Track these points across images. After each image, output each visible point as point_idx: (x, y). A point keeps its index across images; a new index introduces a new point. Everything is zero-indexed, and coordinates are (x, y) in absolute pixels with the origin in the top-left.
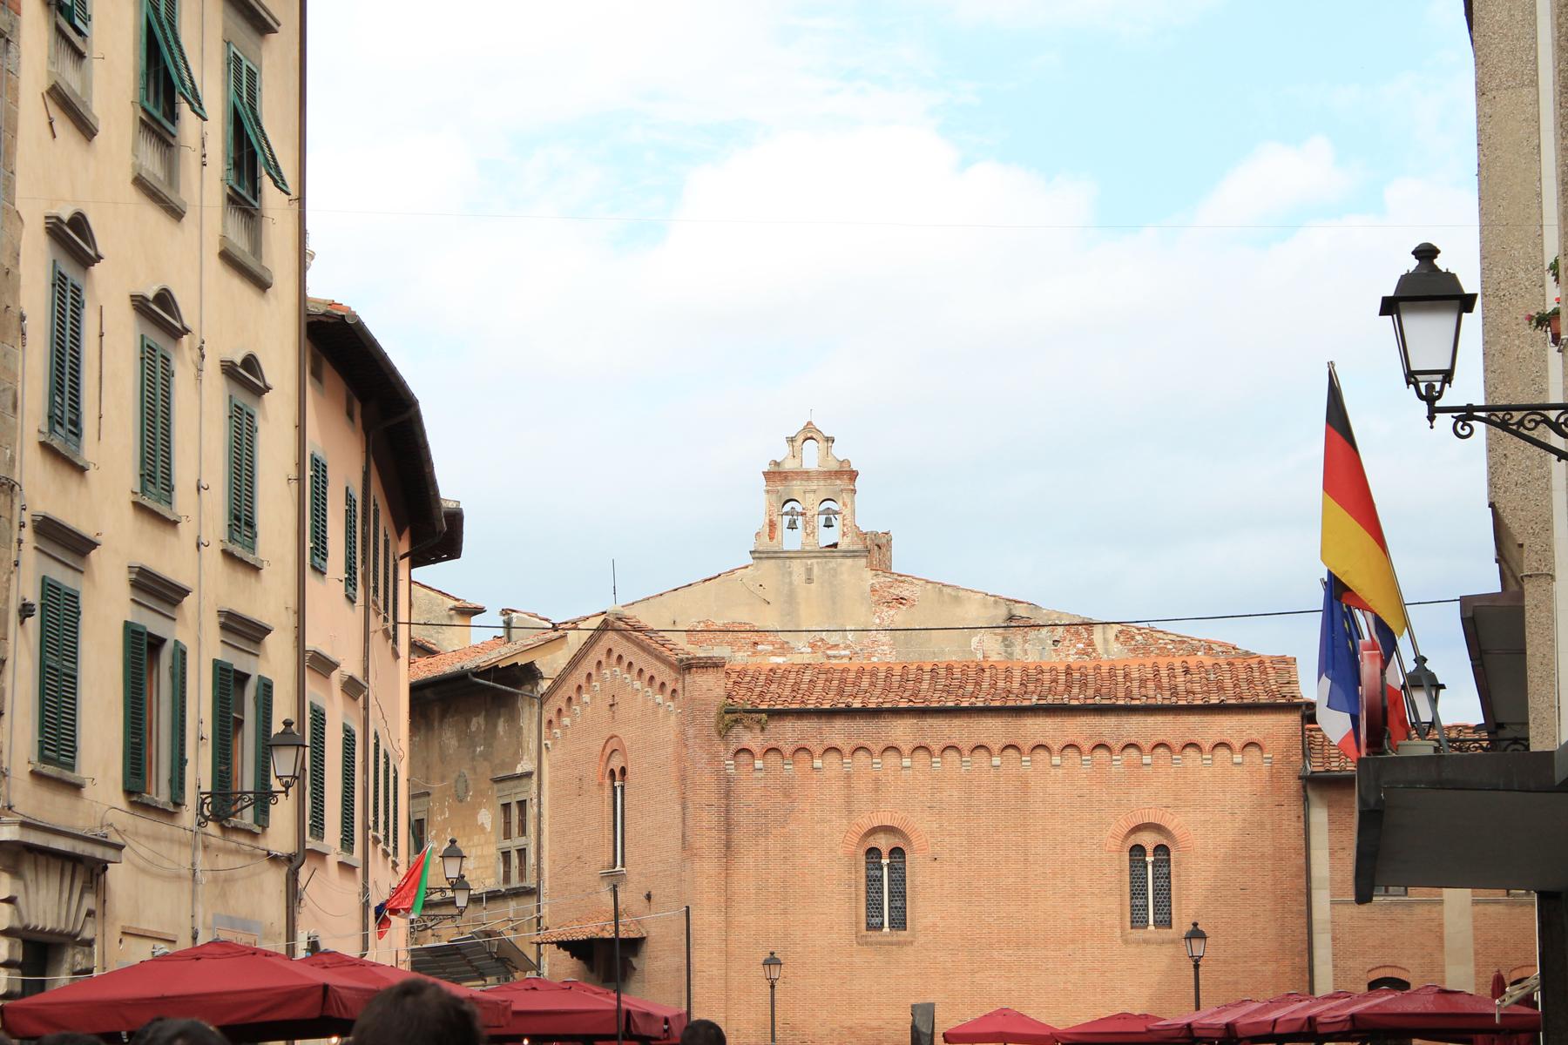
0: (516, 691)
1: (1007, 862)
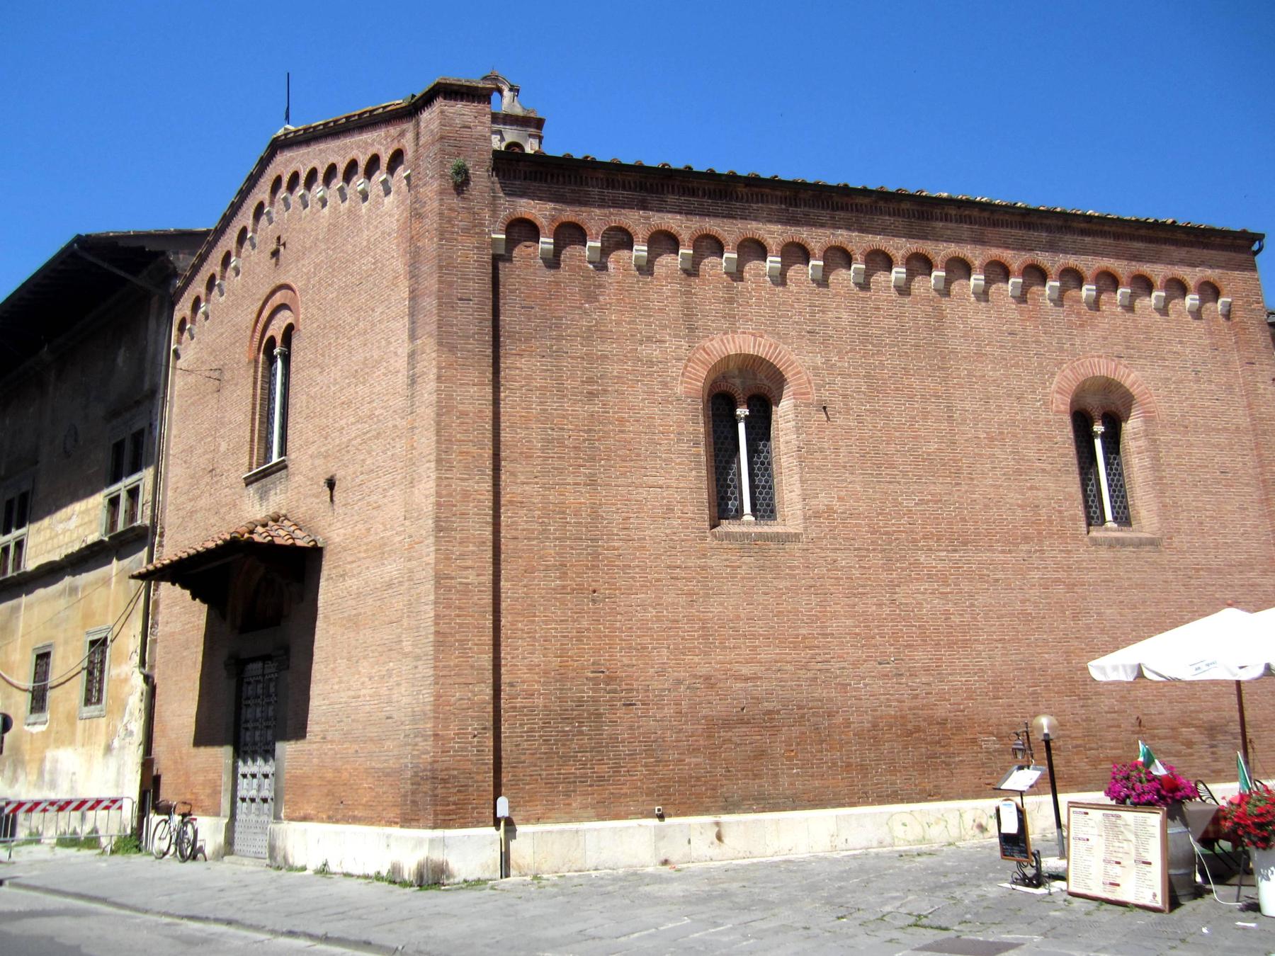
0: (129, 277)
1: (925, 418)
